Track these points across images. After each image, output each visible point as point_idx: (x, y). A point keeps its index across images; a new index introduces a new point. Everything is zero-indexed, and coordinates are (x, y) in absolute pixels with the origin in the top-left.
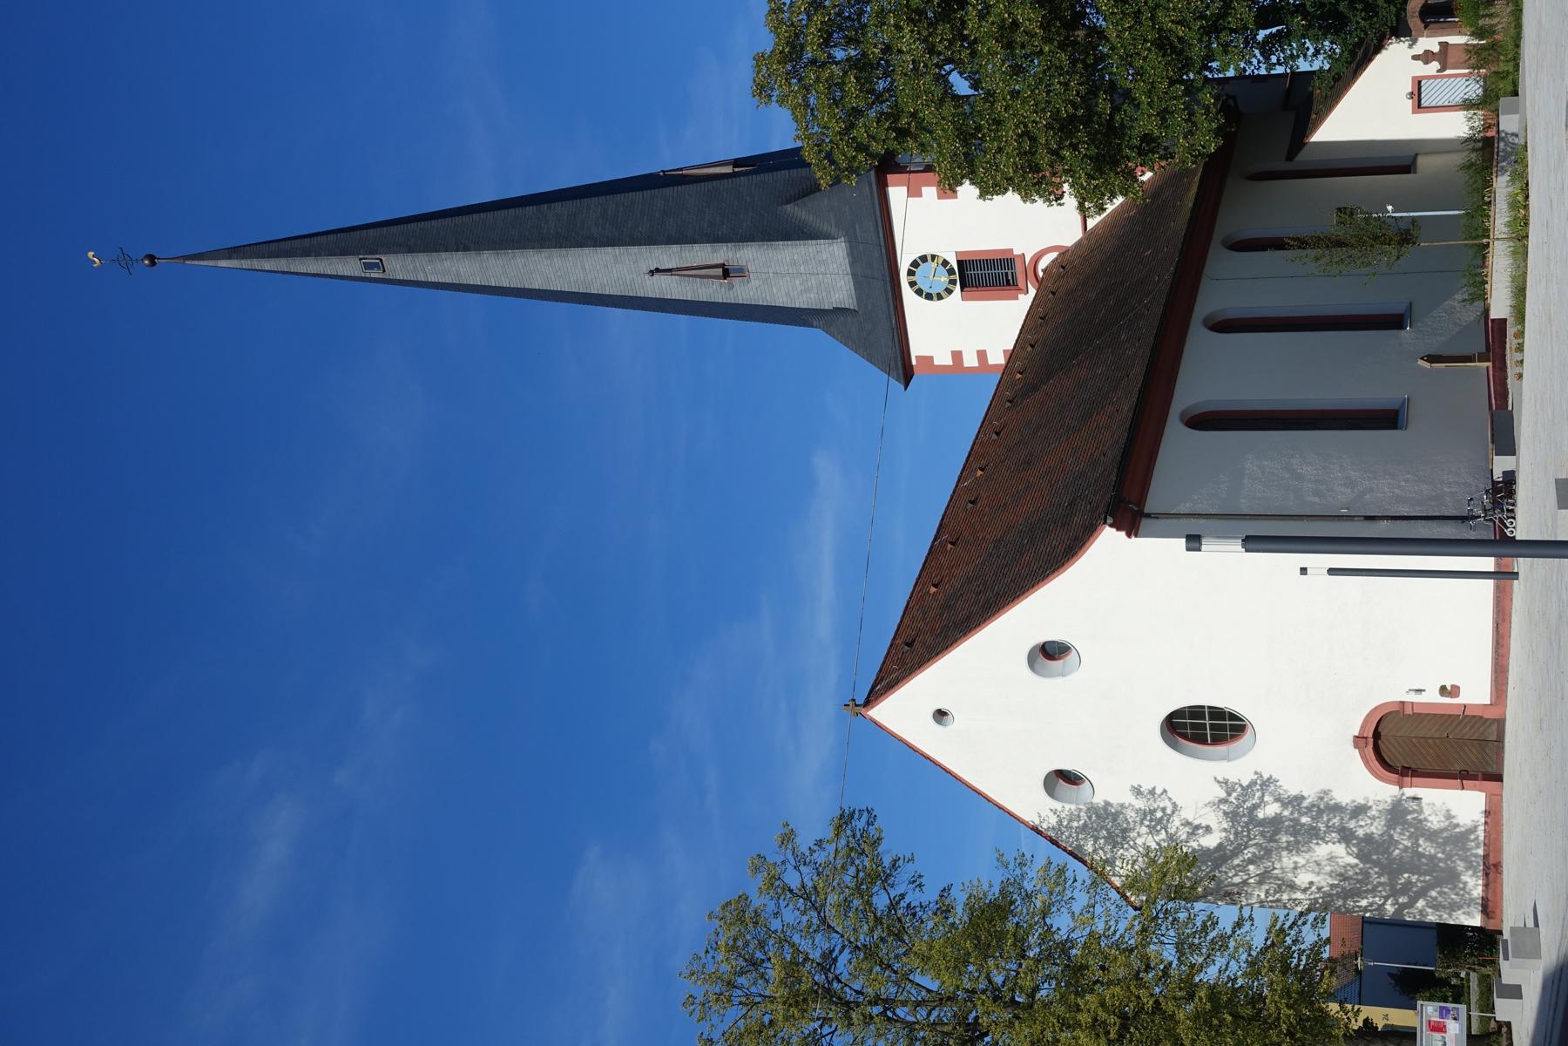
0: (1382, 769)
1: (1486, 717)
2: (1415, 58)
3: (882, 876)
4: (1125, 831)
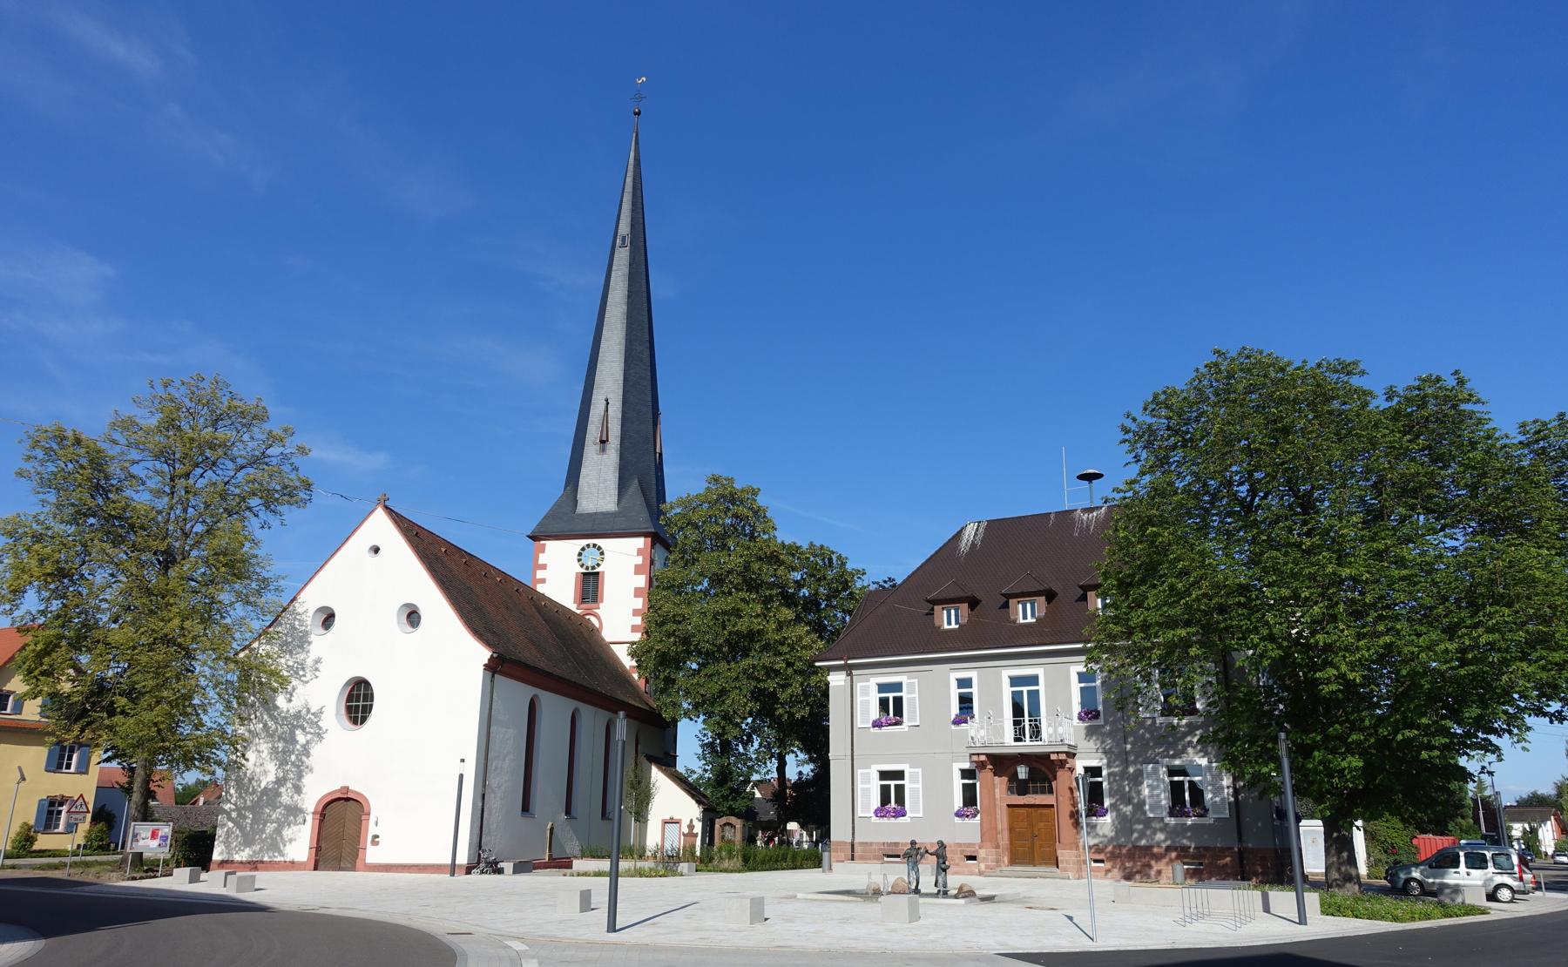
1: (357, 861)
2: (691, 821)
3: (269, 502)
4: (291, 652)
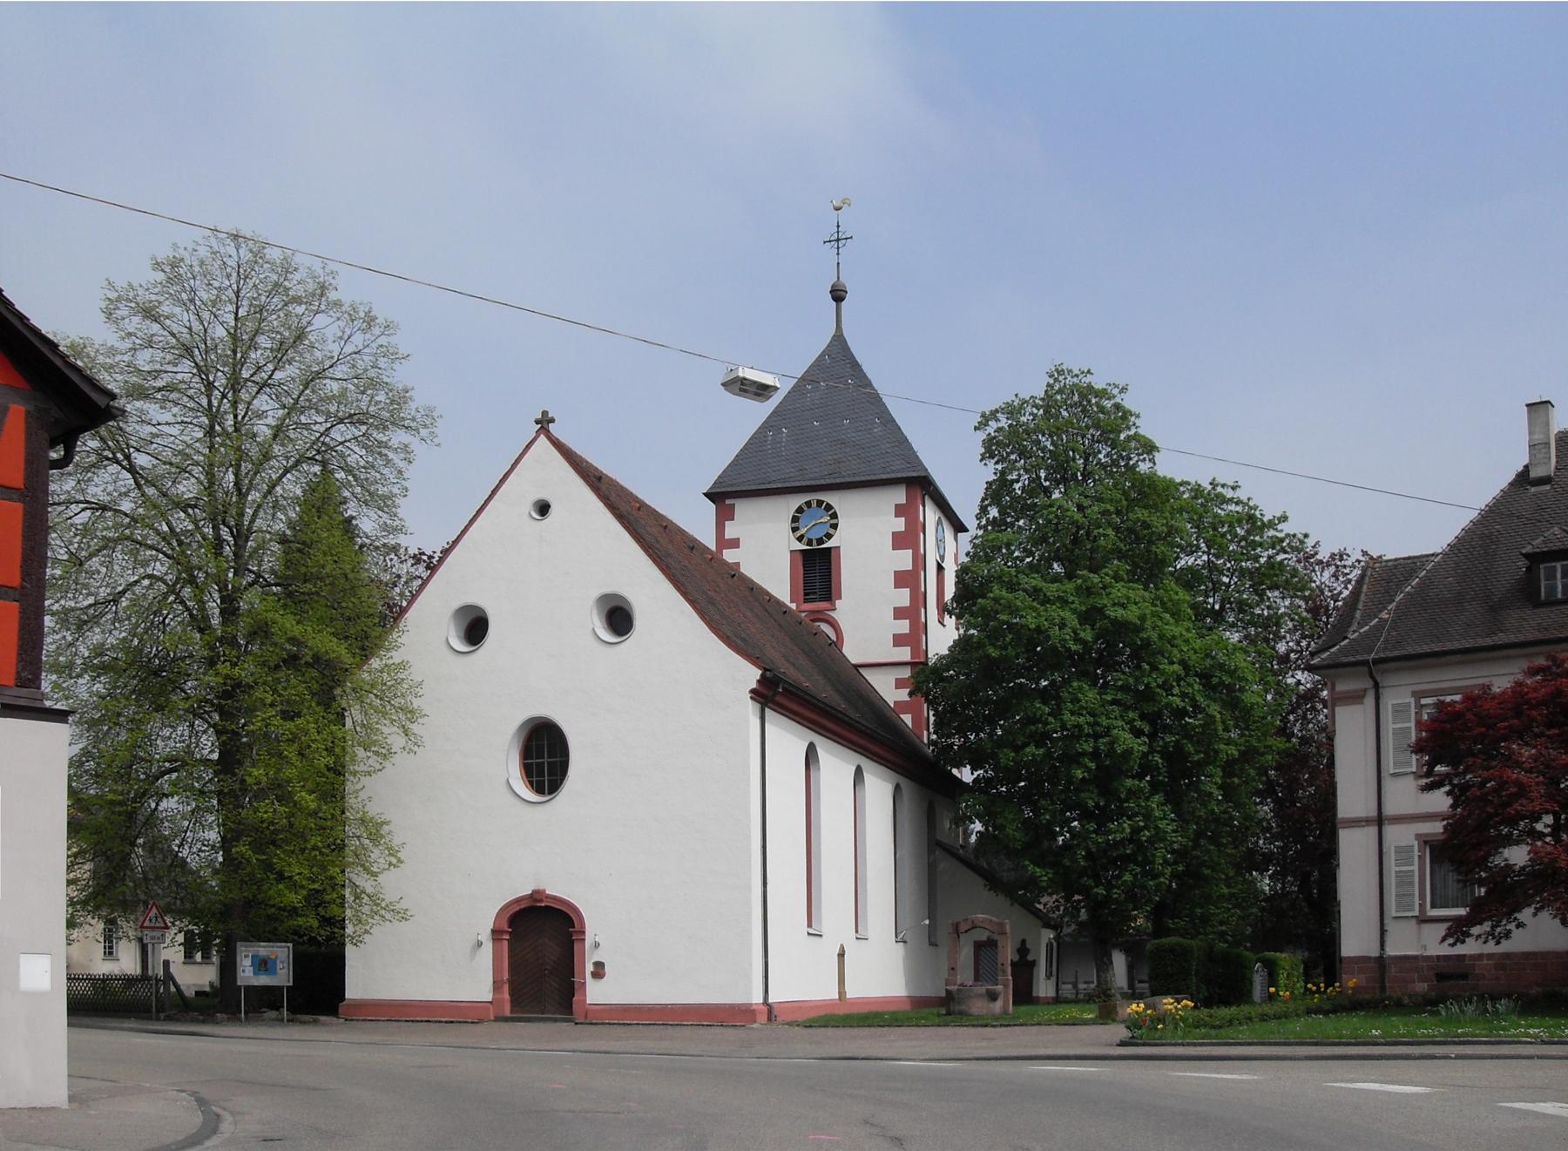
0: (511, 913)
